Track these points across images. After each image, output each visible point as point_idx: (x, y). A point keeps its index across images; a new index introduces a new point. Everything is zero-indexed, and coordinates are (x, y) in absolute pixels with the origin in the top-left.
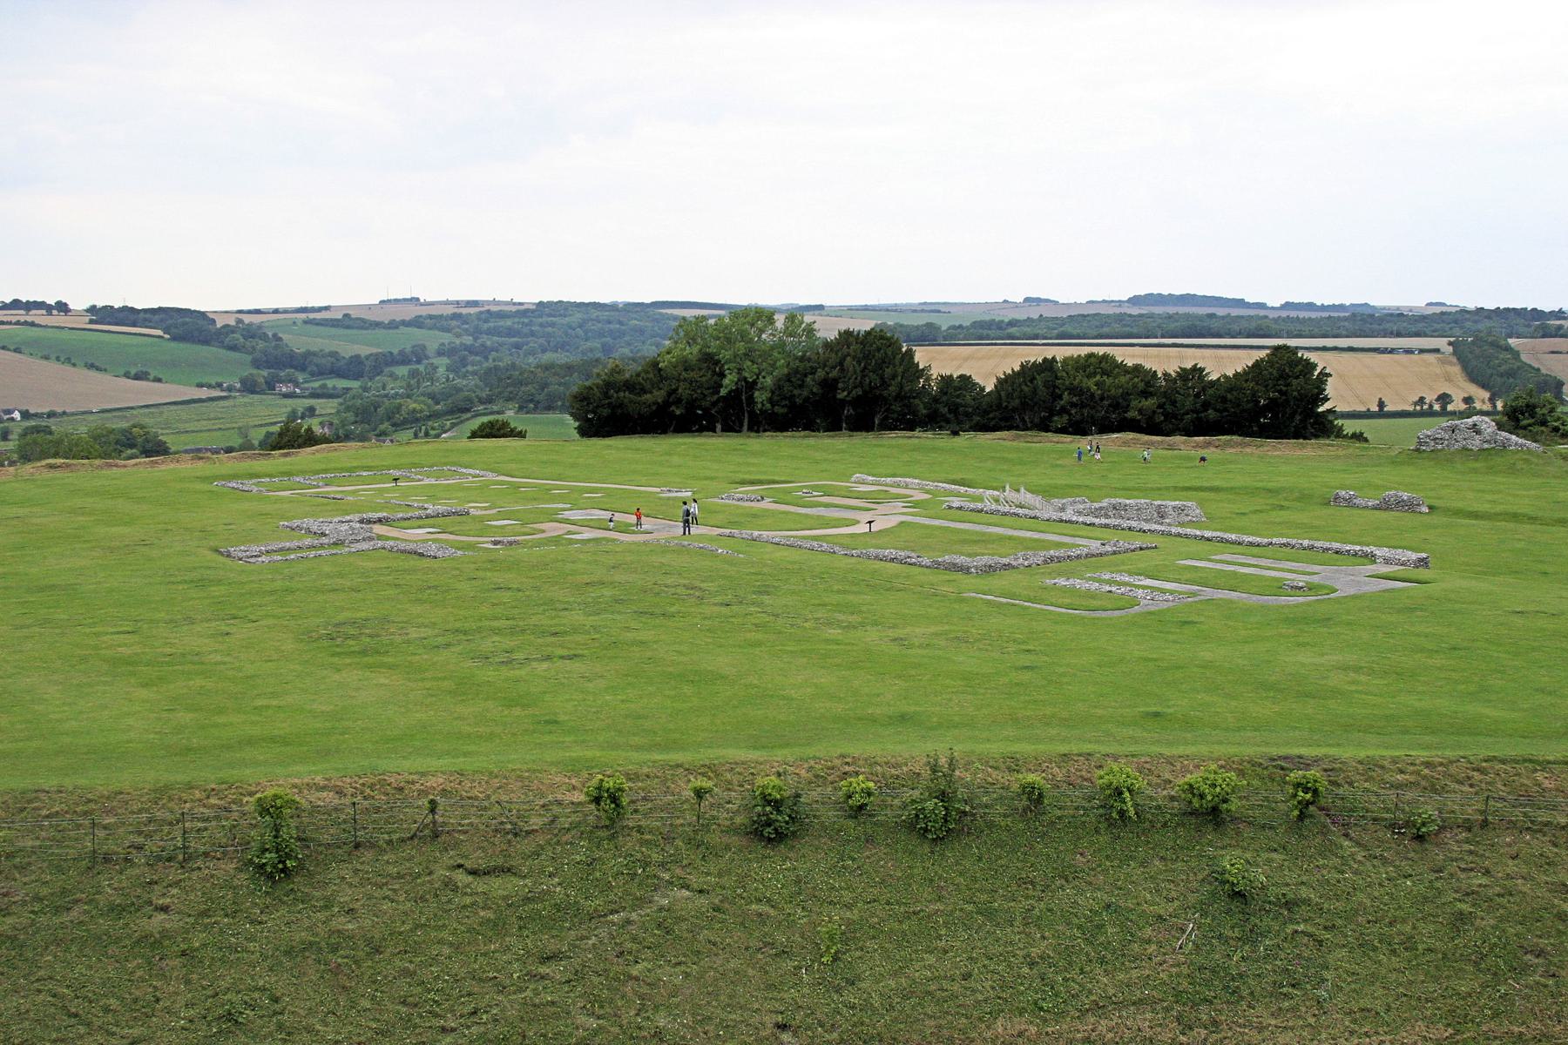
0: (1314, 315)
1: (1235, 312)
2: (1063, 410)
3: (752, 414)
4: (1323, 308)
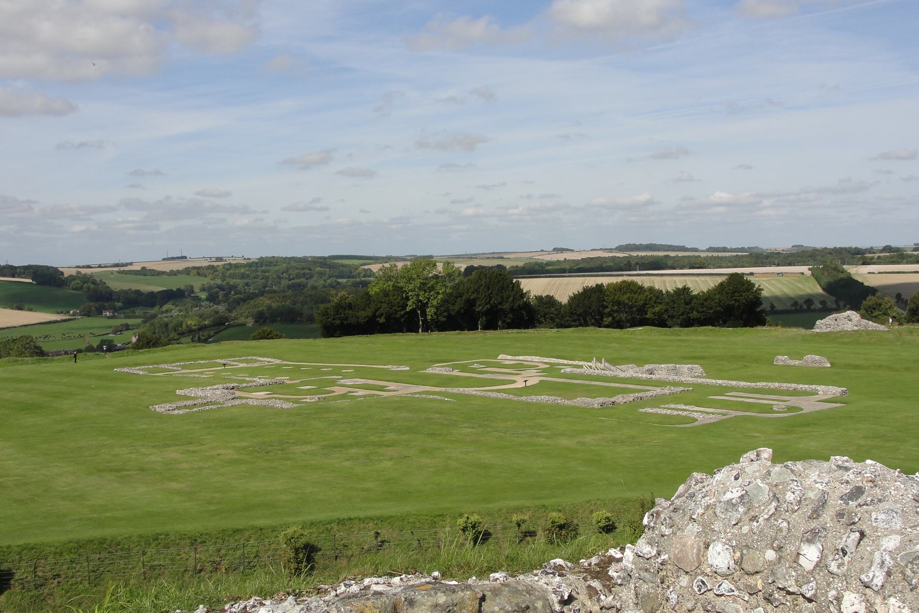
0: (727, 254)
1: (681, 254)
2: (610, 314)
3: (425, 321)
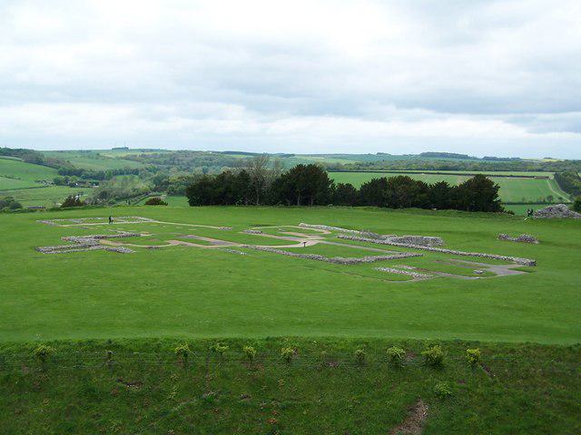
1: (492, 162)
4: (501, 159)
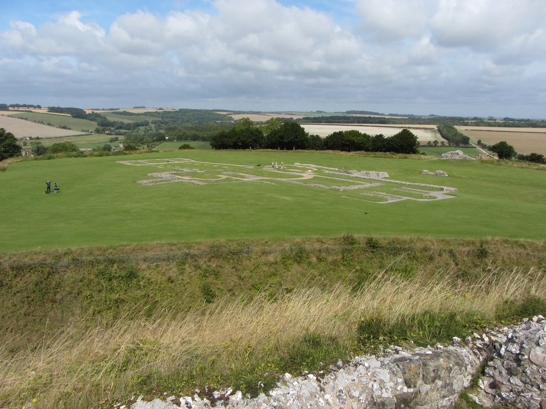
0: (398, 117)
1: (376, 116)
